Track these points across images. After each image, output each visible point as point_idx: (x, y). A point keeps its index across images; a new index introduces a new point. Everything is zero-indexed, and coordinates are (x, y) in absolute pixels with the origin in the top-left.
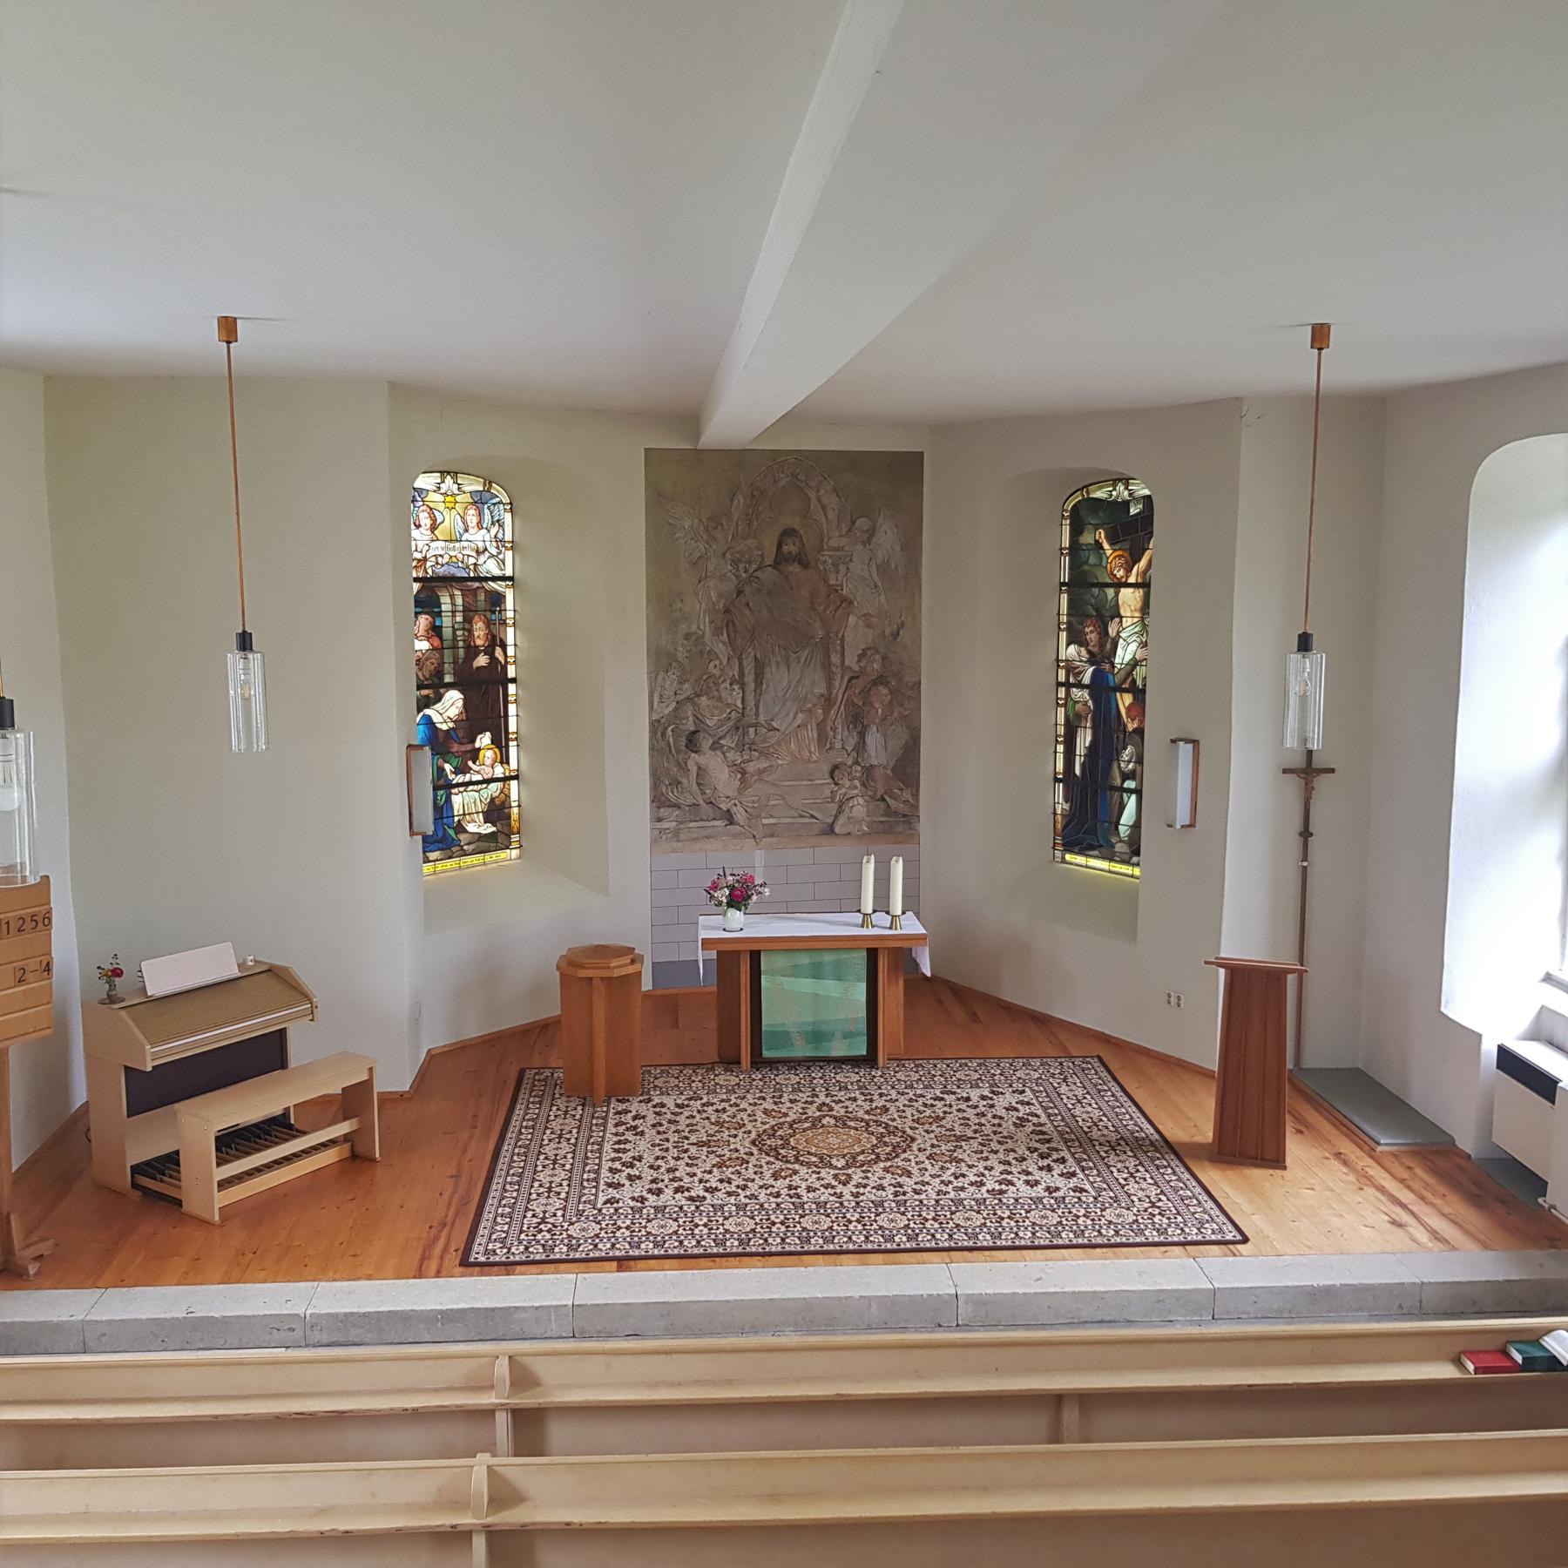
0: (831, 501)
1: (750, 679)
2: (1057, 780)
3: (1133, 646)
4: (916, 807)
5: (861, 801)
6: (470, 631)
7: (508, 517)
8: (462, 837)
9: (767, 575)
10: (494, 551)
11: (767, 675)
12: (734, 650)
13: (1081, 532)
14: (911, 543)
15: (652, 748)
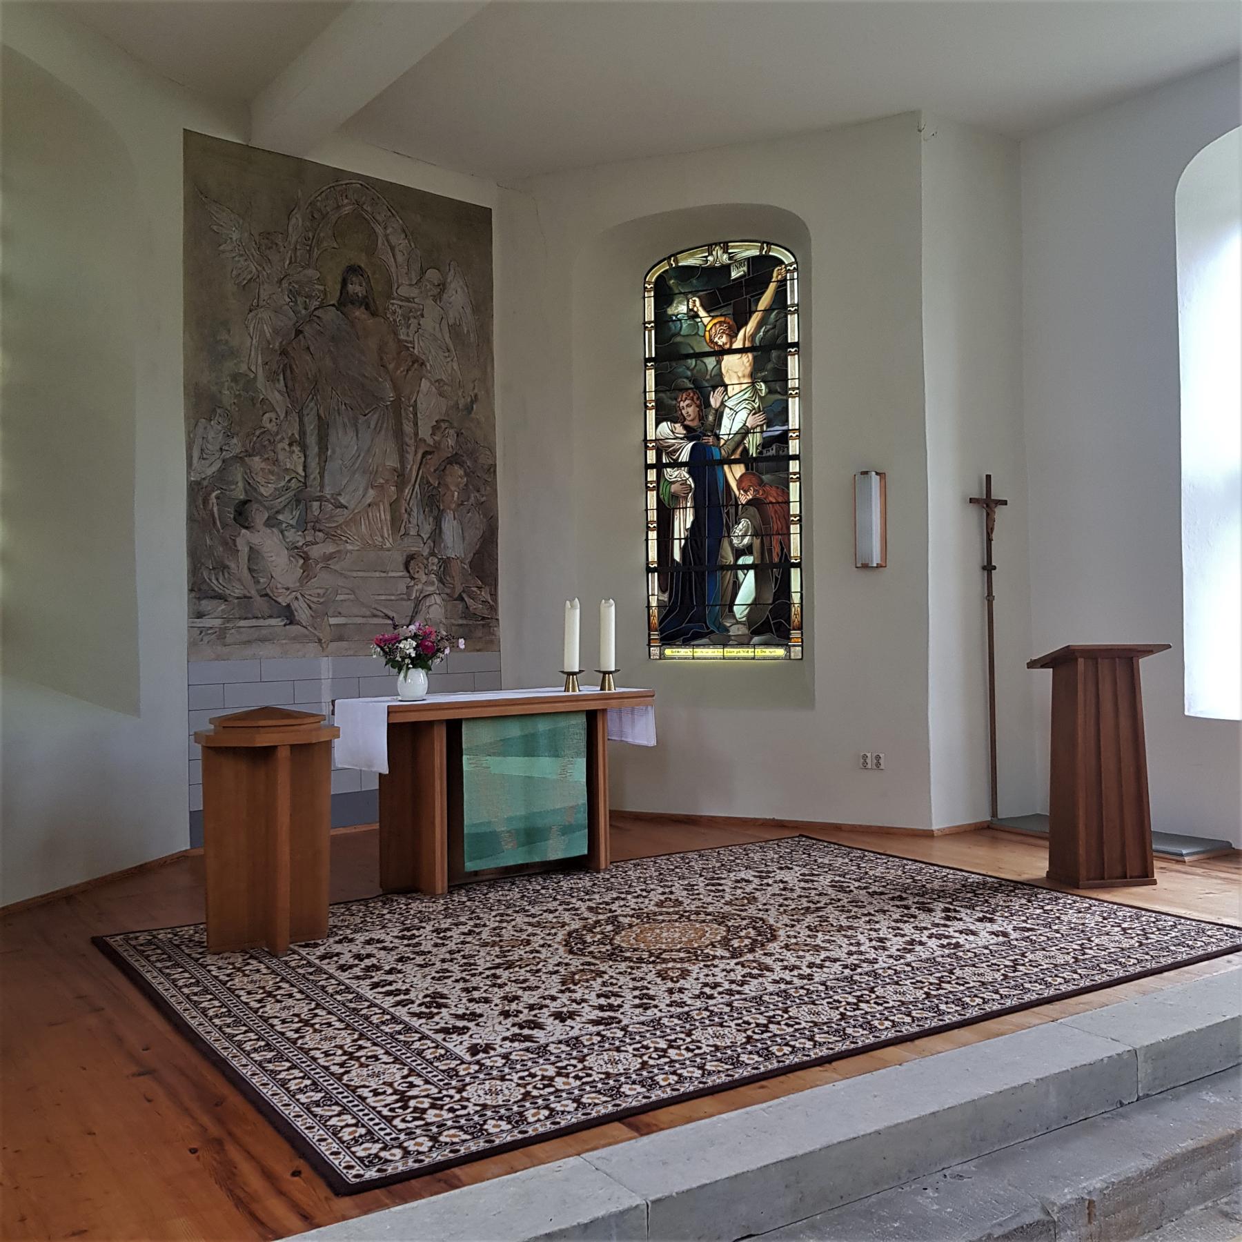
0: (400, 242)
1: (312, 440)
2: (649, 570)
3: (743, 415)
4: (493, 609)
9: (330, 315)
11: (332, 439)
12: (292, 403)
13: (670, 304)
14: (482, 304)
15: (191, 519)
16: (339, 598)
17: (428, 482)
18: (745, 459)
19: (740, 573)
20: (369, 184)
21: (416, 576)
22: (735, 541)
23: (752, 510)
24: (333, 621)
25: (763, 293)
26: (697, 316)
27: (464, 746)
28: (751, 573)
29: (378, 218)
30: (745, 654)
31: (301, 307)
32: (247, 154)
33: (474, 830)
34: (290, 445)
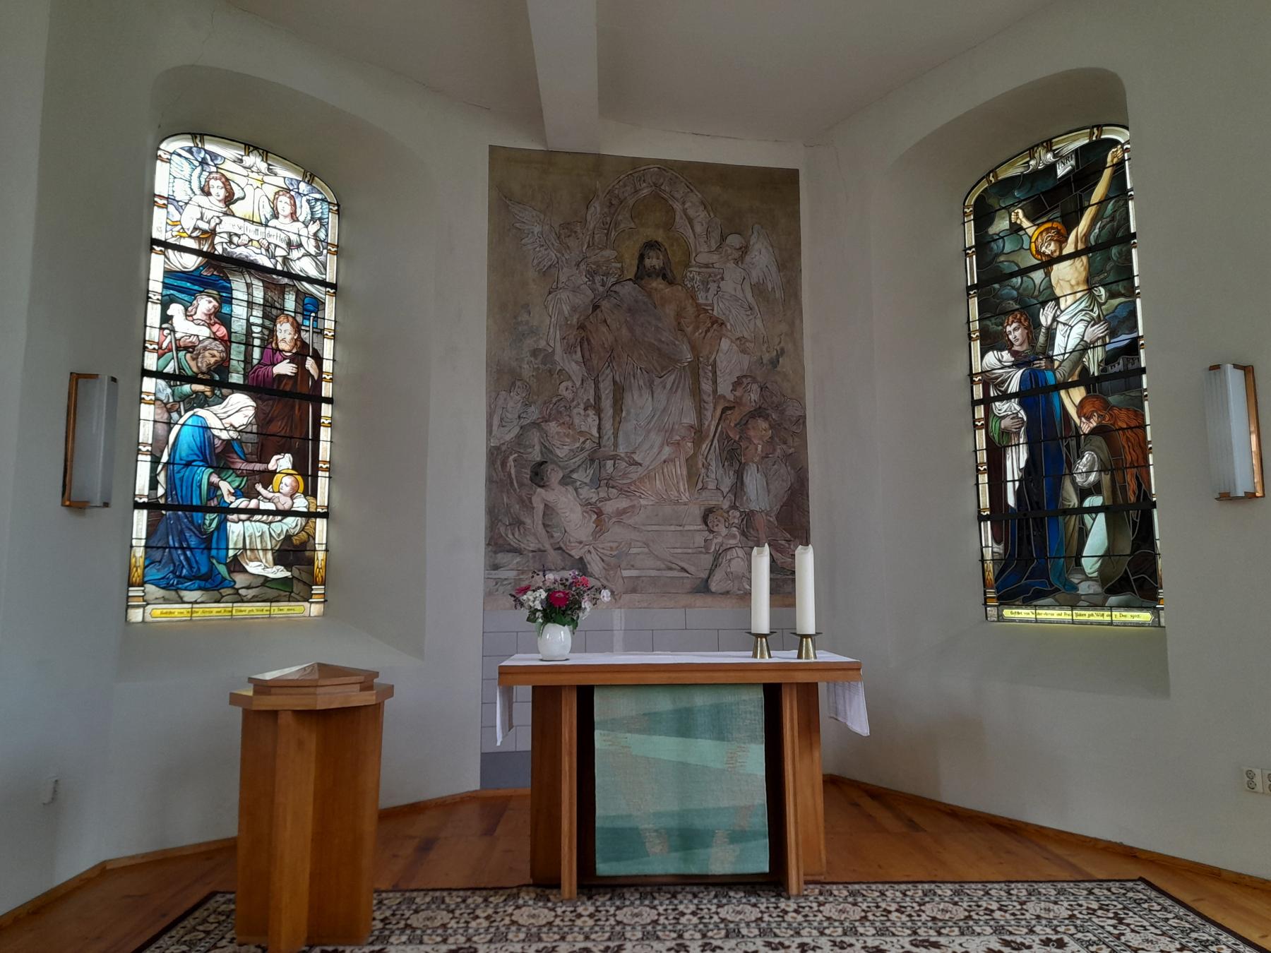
0: (700, 215)
1: (607, 404)
2: (981, 519)
3: (1079, 329)
6: (272, 332)
7: (333, 220)
8: (240, 580)
9: (628, 290)
10: (313, 251)
12: (589, 370)
13: (990, 222)
14: (789, 261)
15: (490, 480)
16: (634, 551)
17: (728, 436)
18: (1085, 379)
19: (1087, 518)
20: (665, 166)
21: (716, 529)
22: (1079, 479)
23: (1098, 441)
24: (626, 573)
25: (1096, 184)
26: (1021, 228)
27: (596, 718)
28: (1101, 517)
29: (676, 195)
30: (1100, 618)
31: (598, 285)
32: (549, 159)
33: (608, 824)
34: (585, 409)
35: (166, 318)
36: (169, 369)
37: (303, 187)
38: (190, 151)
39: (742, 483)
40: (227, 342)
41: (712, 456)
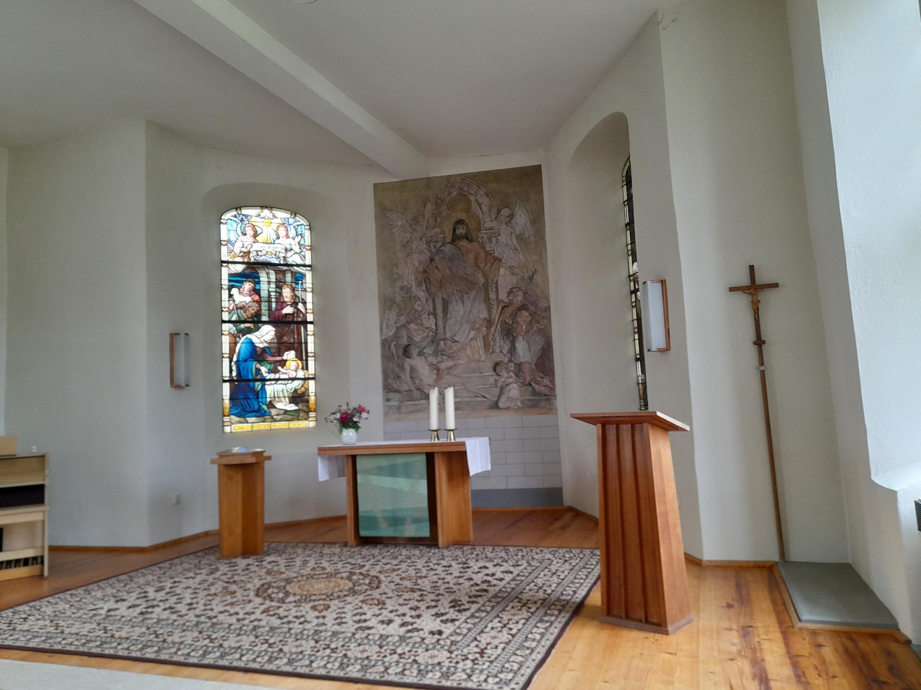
0: (485, 201)
1: (439, 311)
4: (552, 389)
5: (515, 386)
6: (281, 294)
7: (307, 234)
8: (273, 412)
9: (448, 249)
11: (450, 308)
14: (538, 220)
17: (506, 323)
20: (465, 177)
35: (231, 296)
36: (234, 318)
37: (291, 221)
38: (235, 216)
39: (515, 348)
40: (259, 302)
41: (497, 335)
